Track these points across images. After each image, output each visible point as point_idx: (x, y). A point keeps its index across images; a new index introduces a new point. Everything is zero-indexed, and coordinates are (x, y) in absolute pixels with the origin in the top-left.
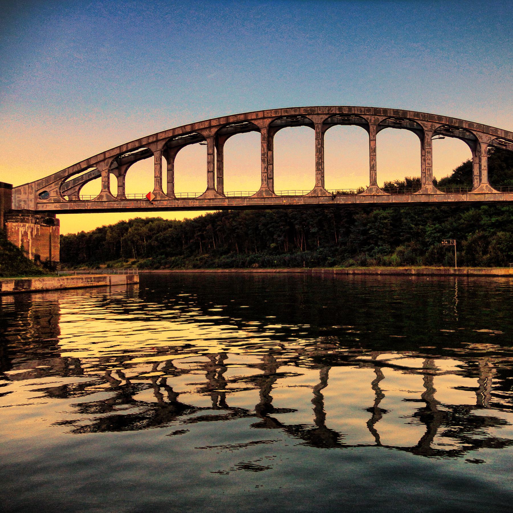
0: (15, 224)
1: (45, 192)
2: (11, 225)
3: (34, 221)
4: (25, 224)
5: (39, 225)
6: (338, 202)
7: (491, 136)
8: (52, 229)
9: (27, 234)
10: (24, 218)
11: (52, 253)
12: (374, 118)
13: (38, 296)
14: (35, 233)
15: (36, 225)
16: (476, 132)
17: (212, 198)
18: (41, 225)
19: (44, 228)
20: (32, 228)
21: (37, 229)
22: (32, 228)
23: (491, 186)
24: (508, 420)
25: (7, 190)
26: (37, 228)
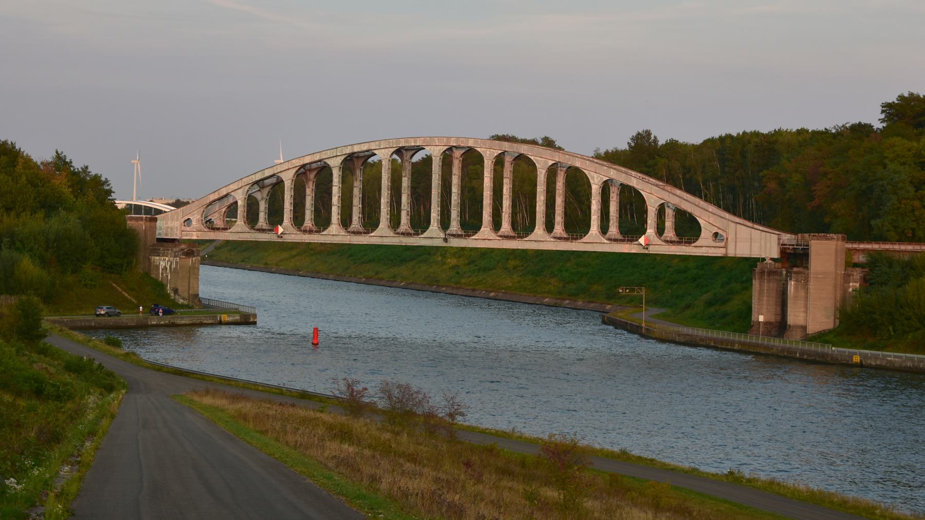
0: (158, 258)
1: (189, 219)
2: (154, 259)
3: (173, 254)
4: (164, 258)
5: (178, 258)
6: (451, 245)
7: (603, 177)
8: (192, 260)
9: (167, 268)
10: (164, 252)
11: (191, 285)
12: (490, 151)
13: (190, 291)
14: (174, 266)
15: (175, 259)
16: (588, 171)
17: (335, 234)
18: (180, 258)
19: (183, 260)
20: (171, 262)
21: (177, 263)
22: (171, 262)
23: (483, 156)
24: (377, 153)
25: (152, 224)
26: (176, 261)
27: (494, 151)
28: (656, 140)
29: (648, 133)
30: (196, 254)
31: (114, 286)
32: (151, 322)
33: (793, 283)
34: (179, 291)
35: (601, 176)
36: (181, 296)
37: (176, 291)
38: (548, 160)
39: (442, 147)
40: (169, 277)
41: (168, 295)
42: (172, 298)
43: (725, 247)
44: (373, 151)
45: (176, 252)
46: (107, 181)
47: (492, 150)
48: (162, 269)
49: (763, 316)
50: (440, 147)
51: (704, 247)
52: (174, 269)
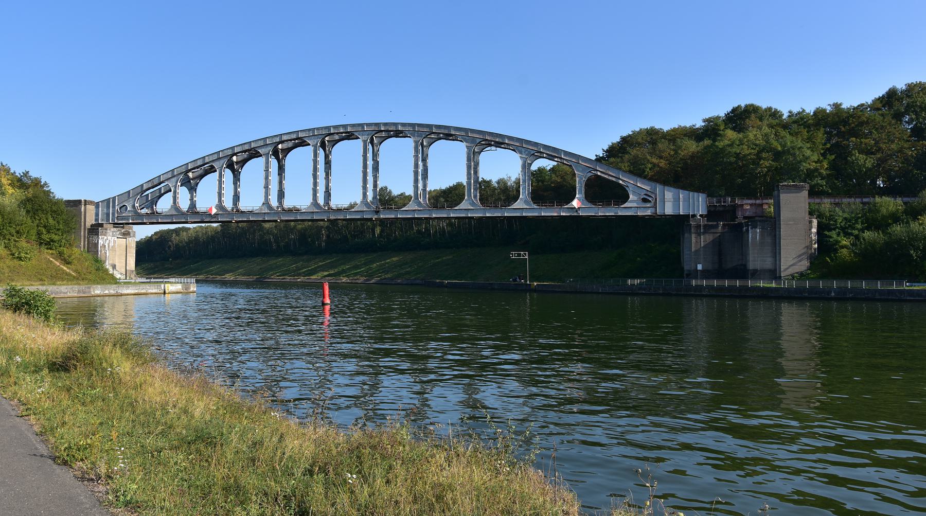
4: (103, 236)
10: (103, 232)
15: (113, 238)
21: (115, 241)
27: (422, 132)
28: (390, 192)
29: (386, 188)
30: (132, 235)
31: (52, 261)
32: (94, 291)
33: (758, 231)
34: (117, 267)
35: (529, 150)
36: (119, 271)
37: (114, 267)
38: (475, 139)
39: (371, 132)
40: (108, 255)
41: (107, 270)
42: (110, 272)
43: (655, 207)
44: (303, 138)
45: (114, 232)
46: (46, 184)
47: (419, 132)
48: (101, 247)
49: (701, 265)
50: (369, 132)
51: (632, 207)
52: (112, 247)
